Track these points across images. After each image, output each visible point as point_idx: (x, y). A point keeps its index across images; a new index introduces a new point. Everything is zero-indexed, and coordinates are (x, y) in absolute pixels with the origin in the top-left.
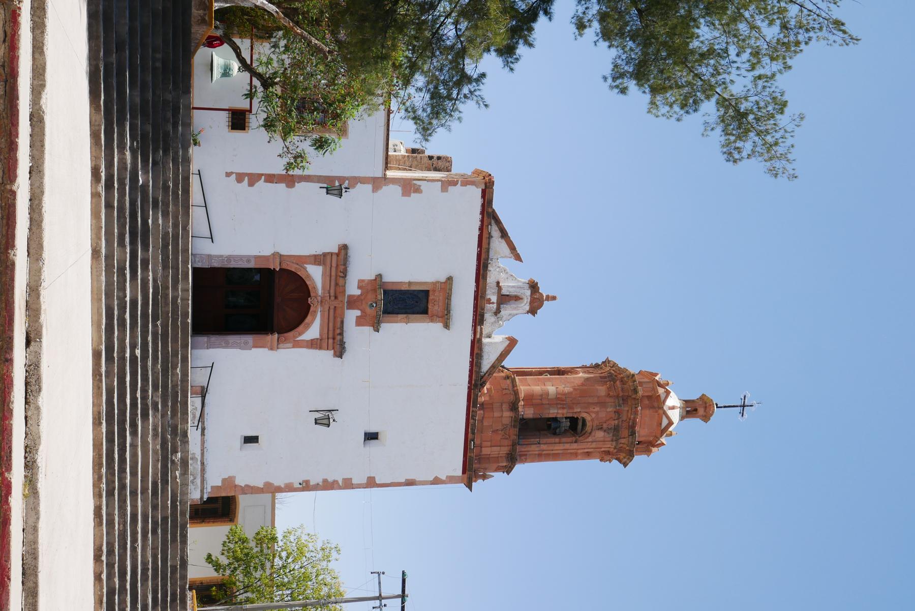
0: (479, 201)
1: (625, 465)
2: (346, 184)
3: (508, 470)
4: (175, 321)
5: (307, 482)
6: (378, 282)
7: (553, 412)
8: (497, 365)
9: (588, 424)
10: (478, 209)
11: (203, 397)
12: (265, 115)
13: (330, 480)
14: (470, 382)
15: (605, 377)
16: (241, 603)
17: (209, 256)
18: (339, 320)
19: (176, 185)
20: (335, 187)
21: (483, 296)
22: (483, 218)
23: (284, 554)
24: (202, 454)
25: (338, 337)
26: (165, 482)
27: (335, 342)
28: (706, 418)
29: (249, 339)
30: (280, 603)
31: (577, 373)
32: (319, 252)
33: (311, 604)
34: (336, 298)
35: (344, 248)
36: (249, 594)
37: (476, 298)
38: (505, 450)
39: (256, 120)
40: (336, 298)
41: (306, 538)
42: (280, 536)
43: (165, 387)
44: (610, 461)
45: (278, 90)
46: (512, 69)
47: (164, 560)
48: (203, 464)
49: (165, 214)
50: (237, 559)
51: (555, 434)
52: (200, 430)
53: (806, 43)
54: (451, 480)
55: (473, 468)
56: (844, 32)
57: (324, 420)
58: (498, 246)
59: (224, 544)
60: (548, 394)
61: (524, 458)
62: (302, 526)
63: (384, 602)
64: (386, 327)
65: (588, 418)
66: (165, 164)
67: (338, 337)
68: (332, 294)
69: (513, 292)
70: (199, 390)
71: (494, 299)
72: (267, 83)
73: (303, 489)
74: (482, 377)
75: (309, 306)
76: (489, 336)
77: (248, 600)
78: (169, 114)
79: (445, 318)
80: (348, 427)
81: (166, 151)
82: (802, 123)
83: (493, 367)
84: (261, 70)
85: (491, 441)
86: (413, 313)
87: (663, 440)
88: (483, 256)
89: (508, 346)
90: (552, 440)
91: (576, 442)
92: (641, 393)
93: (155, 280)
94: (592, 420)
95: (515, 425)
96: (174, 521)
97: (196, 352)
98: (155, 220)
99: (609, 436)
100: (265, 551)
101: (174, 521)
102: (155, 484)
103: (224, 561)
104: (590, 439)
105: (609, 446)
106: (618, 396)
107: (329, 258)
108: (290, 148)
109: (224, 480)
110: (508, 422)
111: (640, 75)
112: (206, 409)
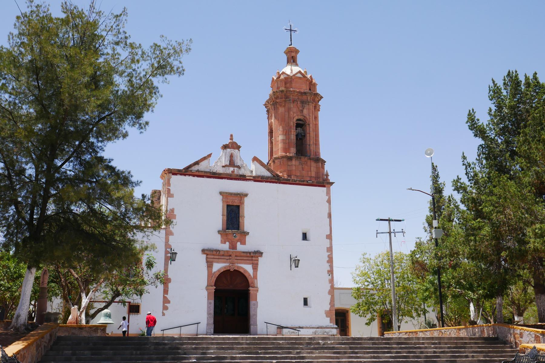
0: (179, 177)
1: (322, 97)
2: (169, 250)
3: (323, 162)
4: (257, 344)
5: (328, 271)
6: (222, 233)
7: (293, 137)
8: (266, 167)
9: (300, 117)
10: (183, 177)
11: (283, 327)
12: (135, 295)
13: (327, 259)
14: (276, 183)
15: (274, 108)
16: (392, 307)
17: (208, 324)
18: (242, 254)
19: (193, 344)
20: (171, 256)
21: (231, 175)
22: (188, 175)
23: (366, 284)
24: (313, 328)
25: (252, 254)
26: (333, 348)
27: (254, 256)
28: (297, 51)
29: (252, 303)
30: (392, 285)
31: (272, 123)
32: (206, 265)
33: (393, 270)
34: (230, 256)
35: (204, 251)
36: (387, 302)
37: (231, 179)
38: (313, 164)
39: (135, 299)
40: (230, 256)
41: (357, 271)
42: (357, 286)
43: (289, 348)
44: (320, 106)
45: (120, 288)
46: (141, 182)
47: (370, 348)
48: (318, 328)
49: (208, 349)
50: (368, 309)
51: (304, 136)
52: (300, 329)
53: (126, 33)
54: (328, 193)
55: (322, 181)
56: (121, 15)
57: (296, 262)
58: (203, 167)
59: (360, 316)
60: (283, 140)
61: (317, 153)
62: (351, 273)
63: (392, 231)
64: (246, 229)
65: (296, 118)
66: (184, 349)
67: (252, 254)
68: (228, 258)
69: (228, 158)
70: (279, 330)
71: (232, 169)
72: (117, 294)
73: (332, 274)
74: (274, 176)
75: (235, 270)
76: (252, 172)
77: (390, 303)
78: (161, 347)
79: (242, 196)
80: (299, 248)
81: (178, 349)
82: (165, 36)
83: (268, 170)
84: (110, 297)
86: (239, 213)
87: (309, 76)
88: (209, 175)
90: (308, 138)
92: (282, 88)
93: (240, 354)
94: (298, 115)
95: (300, 157)
96: (351, 344)
97: (259, 333)
98: (212, 353)
99: (306, 106)
100: (365, 294)
101: (351, 344)
102: (334, 353)
103: (369, 316)
104: (308, 117)
105: (311, 106)
106: (285, 101)
107: (208, 260)
108: (152, 281)
109: (327, 316)
111: (139, 116)
112: (289, 326)
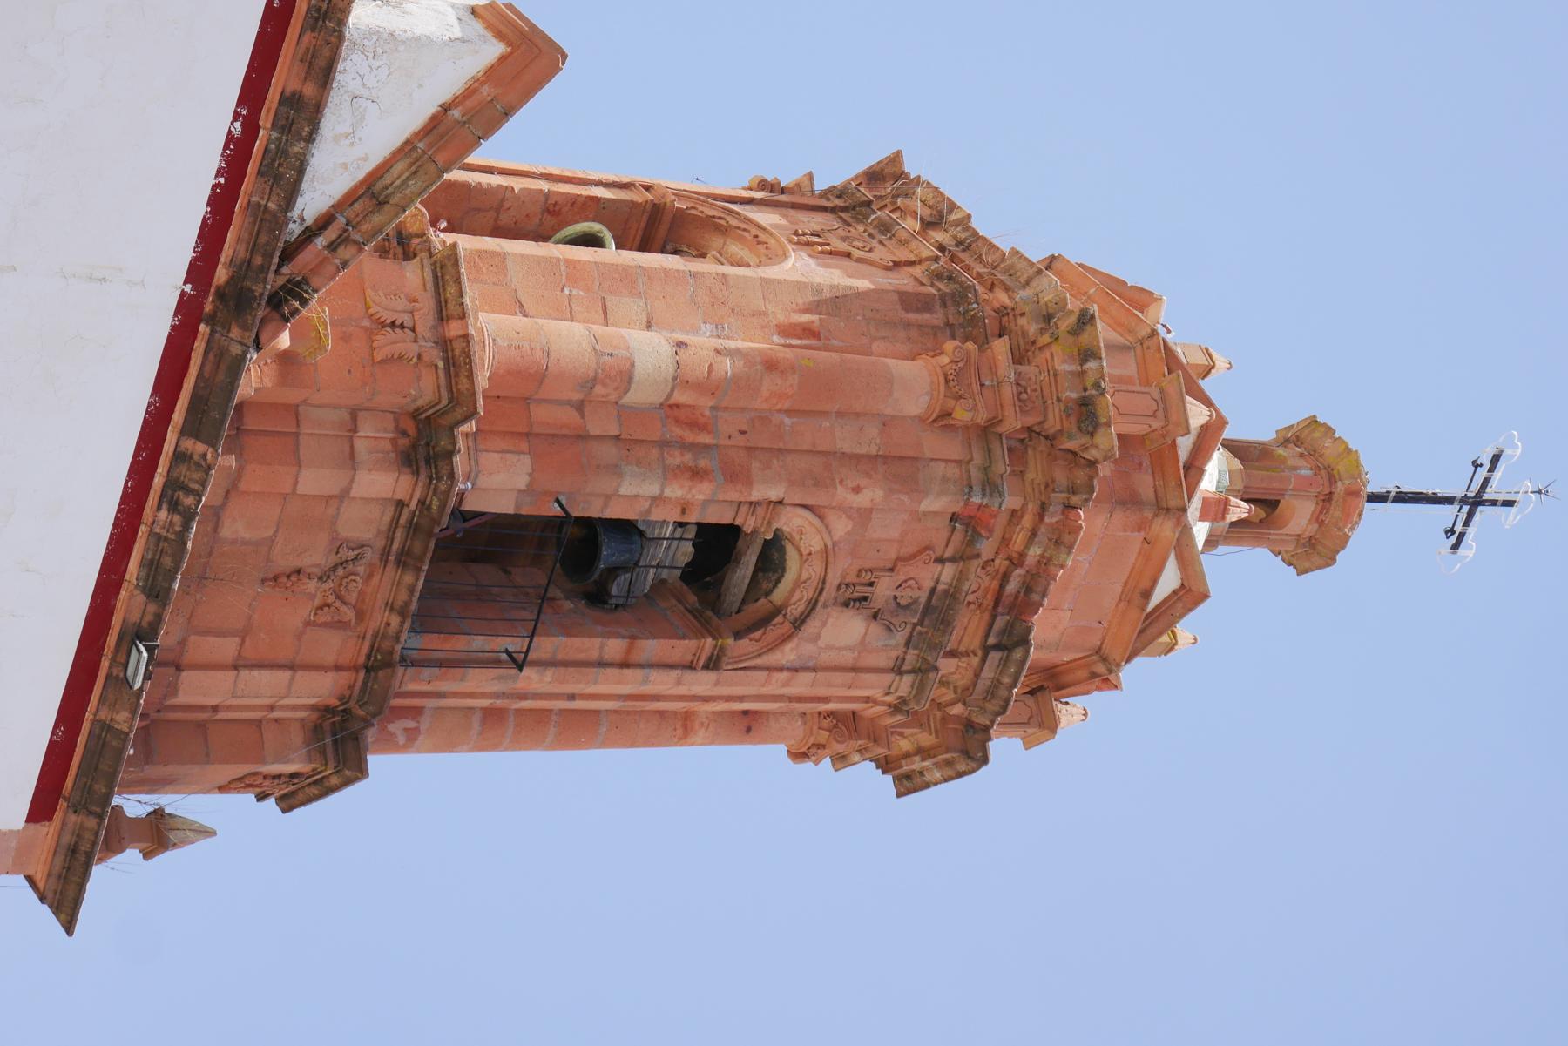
14: (200, 271)
28: (1313, 552)
51: (597, 597)
60: (625, 376)
61: (415, 726)
74: (288, 254)
85: (243, 634)
89: (491, 73)
91: (713, 664)
94: (826, 555)
99: (885, 645)
104: (787, 654)
105: (874, 692)
106: (986, 432)
110: (366, 533)
